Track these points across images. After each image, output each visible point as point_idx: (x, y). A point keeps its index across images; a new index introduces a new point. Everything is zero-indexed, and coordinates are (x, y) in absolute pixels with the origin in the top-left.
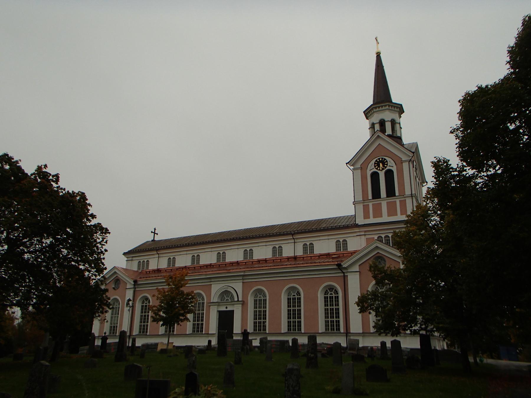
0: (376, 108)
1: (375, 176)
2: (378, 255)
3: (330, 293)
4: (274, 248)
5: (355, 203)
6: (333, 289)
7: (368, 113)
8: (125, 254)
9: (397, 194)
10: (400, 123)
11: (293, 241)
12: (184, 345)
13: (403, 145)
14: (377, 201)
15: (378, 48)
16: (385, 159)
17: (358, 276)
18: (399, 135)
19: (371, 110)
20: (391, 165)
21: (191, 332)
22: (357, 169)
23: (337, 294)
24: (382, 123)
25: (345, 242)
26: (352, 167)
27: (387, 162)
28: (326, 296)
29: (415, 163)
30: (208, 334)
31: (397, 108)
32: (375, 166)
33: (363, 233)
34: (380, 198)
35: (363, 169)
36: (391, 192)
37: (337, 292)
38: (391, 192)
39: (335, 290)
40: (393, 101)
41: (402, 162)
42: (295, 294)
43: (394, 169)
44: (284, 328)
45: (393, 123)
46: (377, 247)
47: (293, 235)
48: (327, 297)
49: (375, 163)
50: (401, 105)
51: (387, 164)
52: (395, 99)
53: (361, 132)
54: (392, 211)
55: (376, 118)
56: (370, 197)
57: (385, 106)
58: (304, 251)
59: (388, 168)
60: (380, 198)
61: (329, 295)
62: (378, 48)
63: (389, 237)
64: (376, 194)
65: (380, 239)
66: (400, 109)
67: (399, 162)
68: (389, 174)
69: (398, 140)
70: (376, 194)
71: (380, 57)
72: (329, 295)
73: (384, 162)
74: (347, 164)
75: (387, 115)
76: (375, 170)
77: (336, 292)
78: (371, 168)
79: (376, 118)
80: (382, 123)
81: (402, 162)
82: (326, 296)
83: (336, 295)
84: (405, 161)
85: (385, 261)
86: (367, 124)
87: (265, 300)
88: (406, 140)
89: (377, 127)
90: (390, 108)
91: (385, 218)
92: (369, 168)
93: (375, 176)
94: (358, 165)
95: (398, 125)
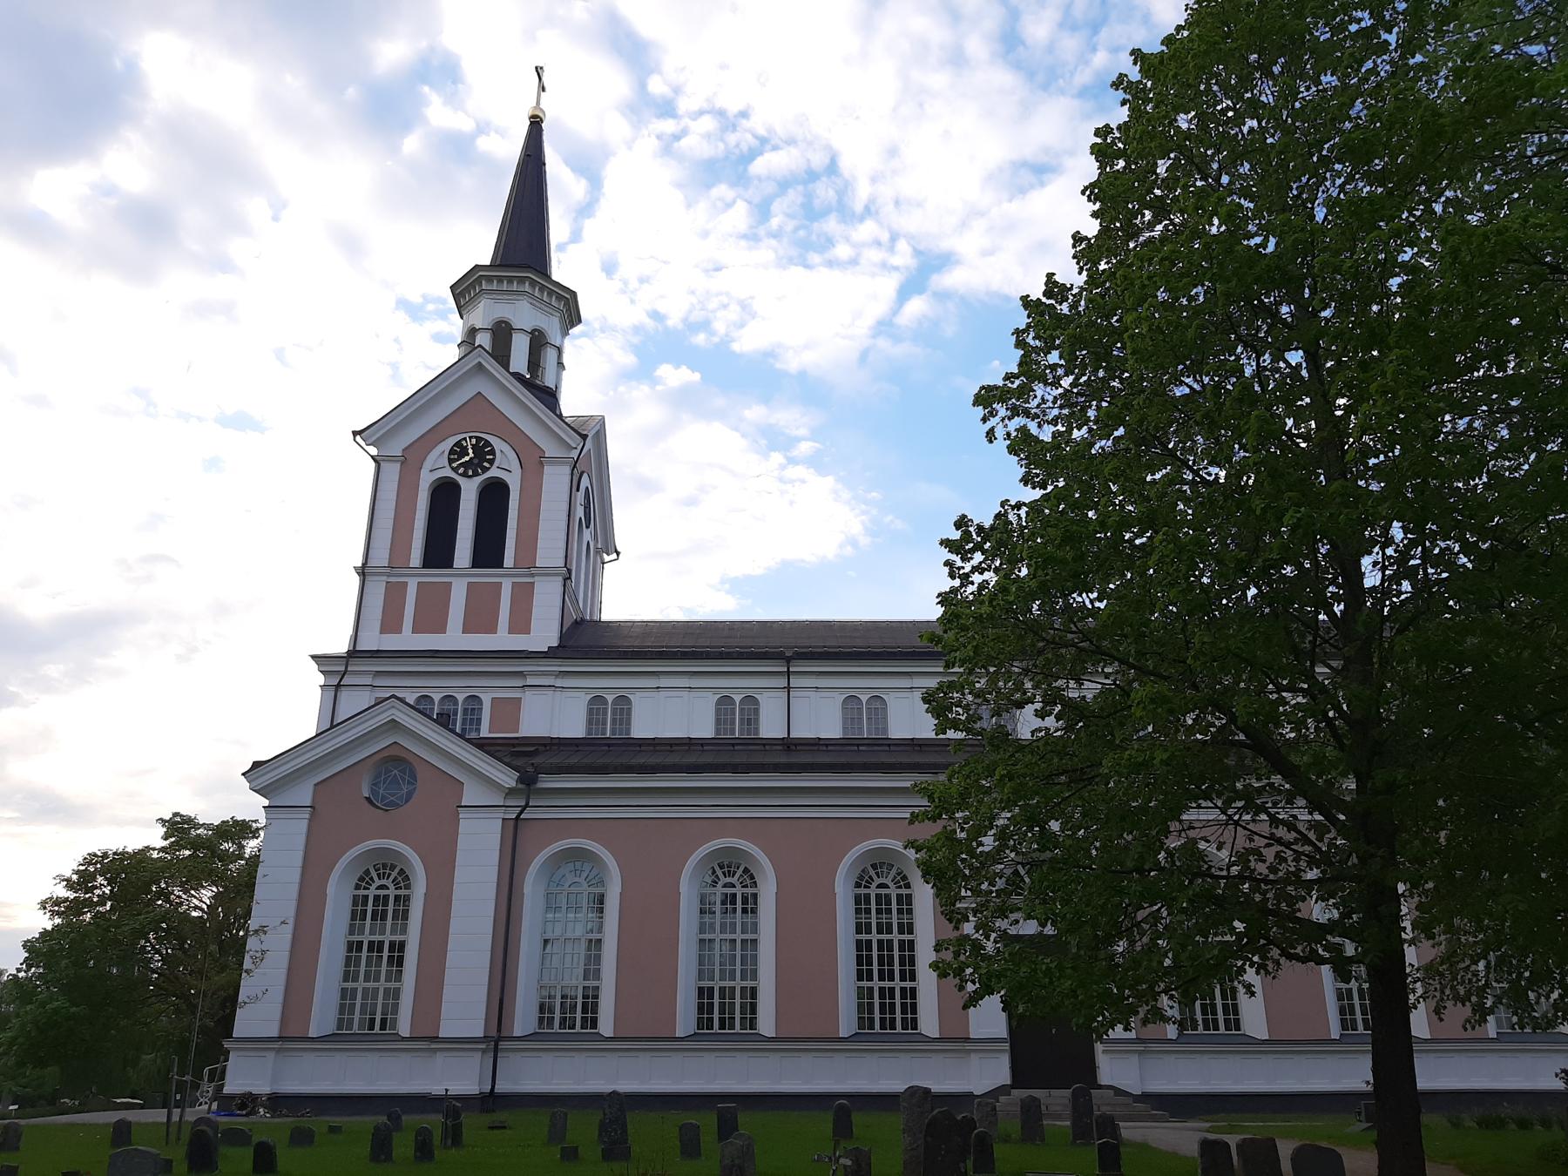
0: (489, 279)
1: (445, 494)
2: (394, 752)
3: (723, 880)
4: (598, 700)
5: (363, 572)
6: (393, 867)
7: (466, 290)
8: (314, 657)
9: (509, 560)
10: (560, 350)
11: (783, 682)
12: (604, 1087)
13: (560, 416)
14: (436, 576)
15: (538, 102)
16: (487, 443)
17: (304, 825)
18: (549, 382)
19: (472, 285)
20: (507, 467)
21: (330, 1028)
22: (391, 459)
23: (408, 887)
24: (502, 332)
25: (623, 702)
26: (373, 451)
27: (492, 452)
28: (862, 891)
29: (585, 482)
30: (435, 1039)
31: (560, 297)
32: (451, 461)
33: (368, 680)
34: (501, 566)
35: (410, 461)
36: (488, 552)
37: (905, 878)
38: (488, 552)
39: (402, 872)
40: (557, 275)
41: (541, 460)
42: (888, 881)
43: (514, 481)
44: (463, 1012)
45: (538, 342)
46: (393, 725)
47: (788, 660)
48: (868, 897)
49: (452, 452)
50: (574, 294)
51: (491, 462)
52: (562, 270)
53: (432, 347)
54: (480, 617)
55: (484, 313)
56: (416, 557)
57: (521, 280)
58: (885, 718)
59: (494, 472)
60: (501, 566)
61: (372, 892)
62: (538, 102)
63: (605, 701)
64: (438, 553)
65: (422, 707)
66: (568, 308)
67: (533, 462)
68: (494, 495)
69: (550, 397)
70: (438, 553)
71: (541, 130)
72: (372, 892)
73: (484, 453)
74: (355, 433)
75: (524, 314)
76: (448, 473)
77: (404, 879)
78: (436, 466)
79: (484, 313)
80: (502, 332)
81: (541, 460)
82: (862, 891)
83: (904, 891)
84: (555, 461)
85: (414, 776)
86: (455, 326)
87: (403, 901)
88: (573, 403)
89: (484, 340)
90: (527, 287)
91: (454, 638)
92: (428, 465)
93: (445, 494)
94: (396, 449)
95: (550, 354)
